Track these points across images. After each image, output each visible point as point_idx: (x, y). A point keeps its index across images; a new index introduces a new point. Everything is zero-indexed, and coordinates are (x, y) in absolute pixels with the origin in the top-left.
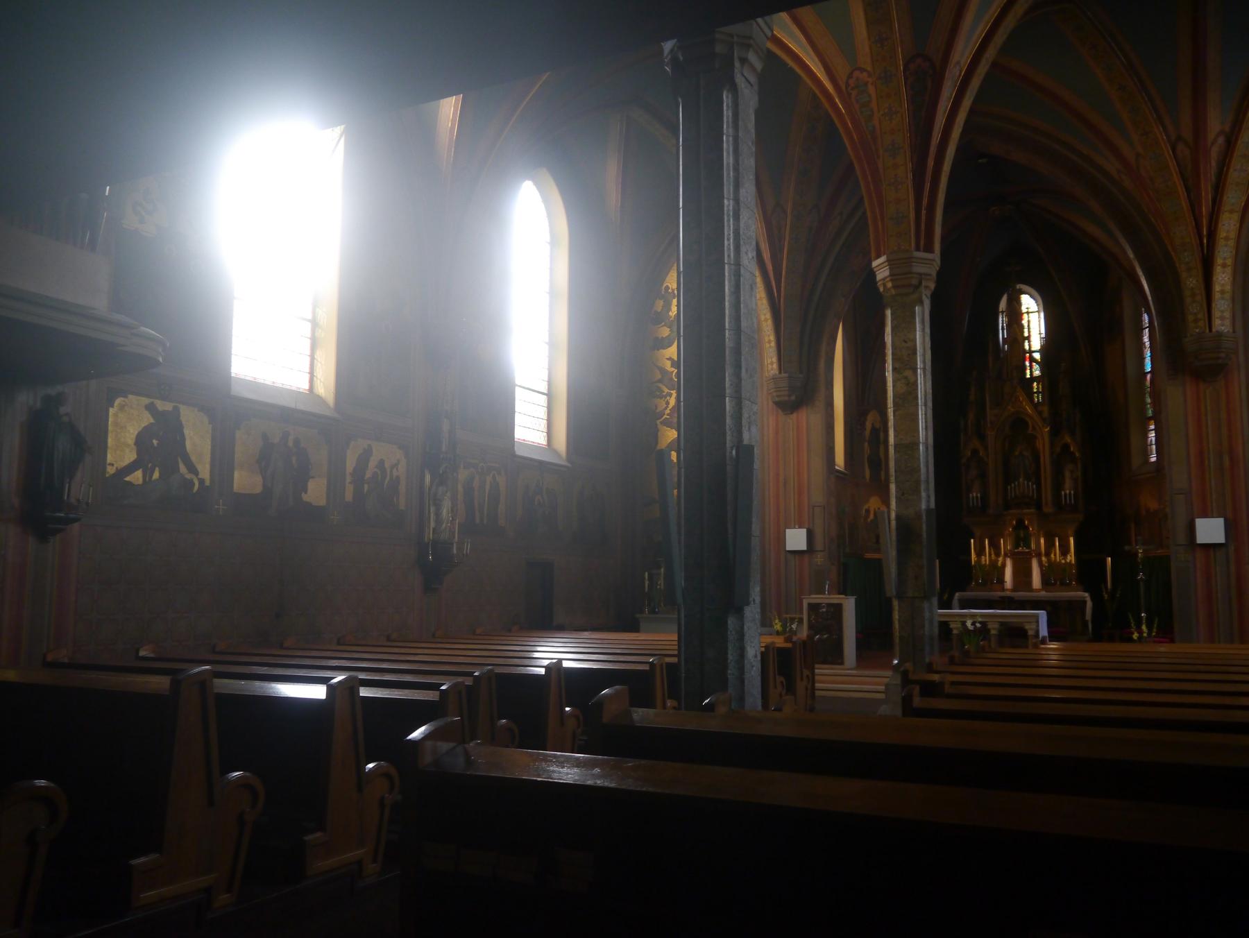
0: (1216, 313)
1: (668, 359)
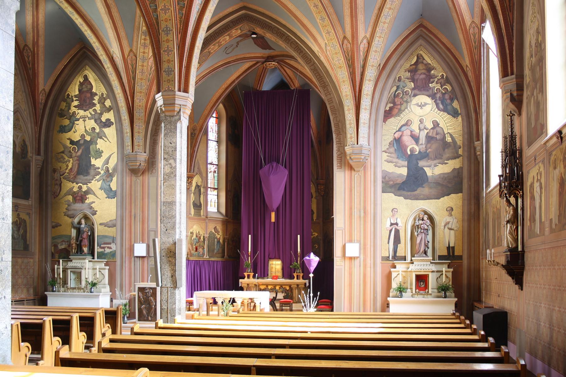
0: (360, 134)
1: (68, 139)
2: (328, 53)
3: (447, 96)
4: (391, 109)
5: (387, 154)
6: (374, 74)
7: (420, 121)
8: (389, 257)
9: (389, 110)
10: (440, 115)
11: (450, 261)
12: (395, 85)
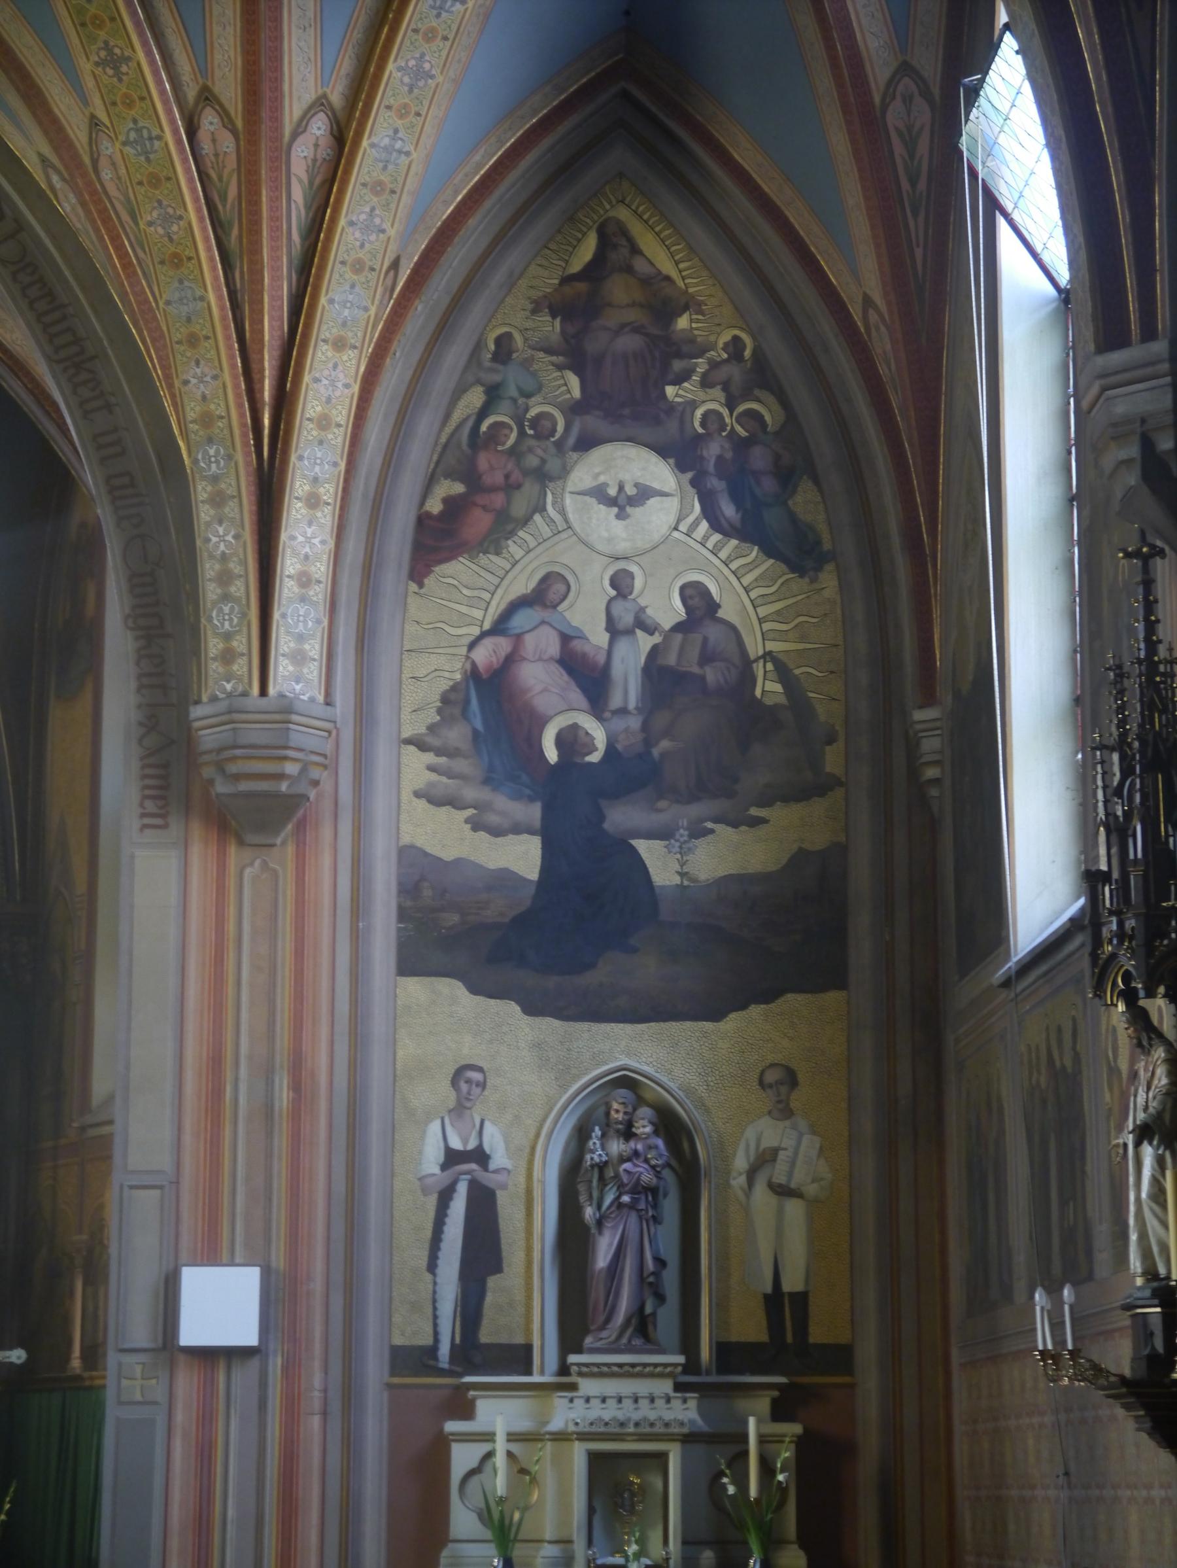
0: (282, 642)
2: (107, 175)
3: (759, 458)
4: (454, 507)
5: (429, 758)
6: (366, 309)
7: (614, 584)
8: (433, 1351)
9: (442, 514)
10: (723, 554)
11: (782, 1380)
12: (479, 382)
